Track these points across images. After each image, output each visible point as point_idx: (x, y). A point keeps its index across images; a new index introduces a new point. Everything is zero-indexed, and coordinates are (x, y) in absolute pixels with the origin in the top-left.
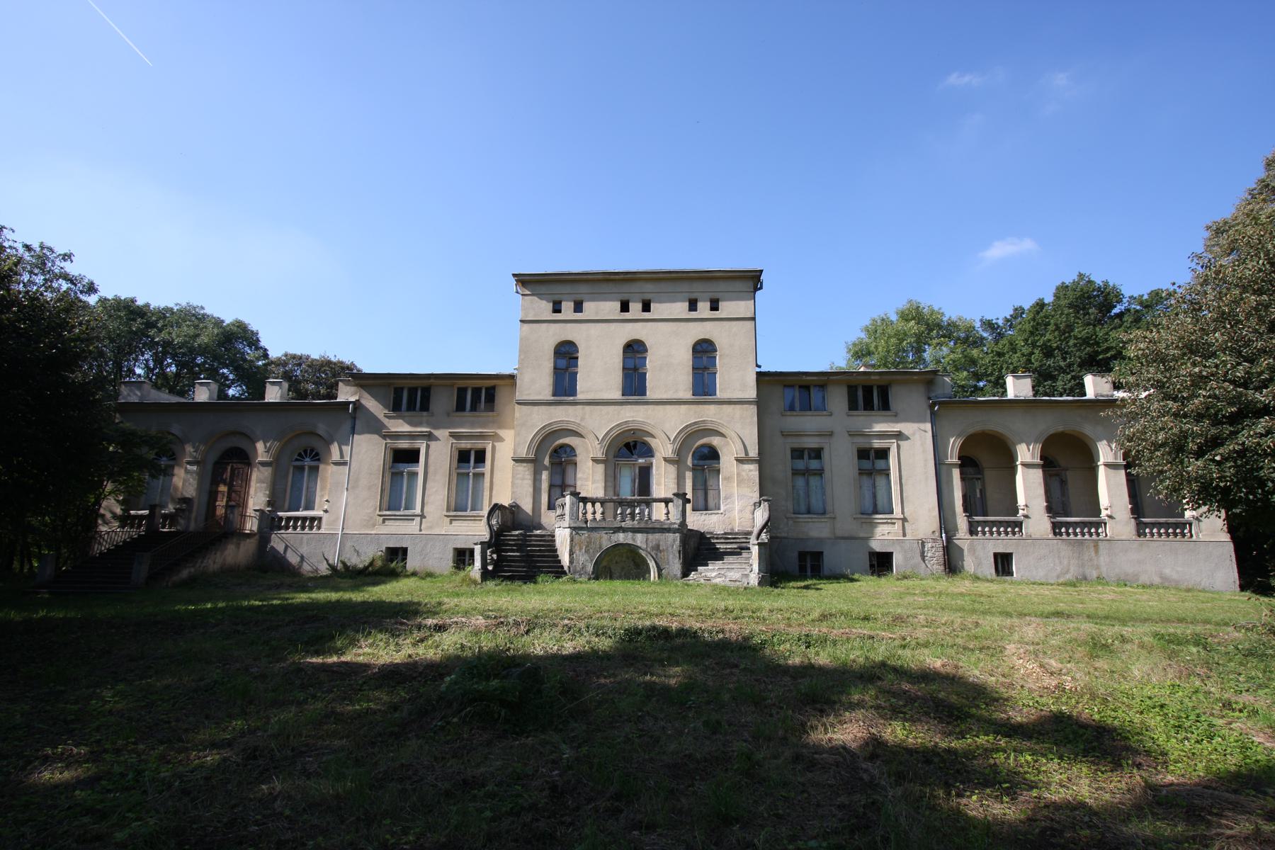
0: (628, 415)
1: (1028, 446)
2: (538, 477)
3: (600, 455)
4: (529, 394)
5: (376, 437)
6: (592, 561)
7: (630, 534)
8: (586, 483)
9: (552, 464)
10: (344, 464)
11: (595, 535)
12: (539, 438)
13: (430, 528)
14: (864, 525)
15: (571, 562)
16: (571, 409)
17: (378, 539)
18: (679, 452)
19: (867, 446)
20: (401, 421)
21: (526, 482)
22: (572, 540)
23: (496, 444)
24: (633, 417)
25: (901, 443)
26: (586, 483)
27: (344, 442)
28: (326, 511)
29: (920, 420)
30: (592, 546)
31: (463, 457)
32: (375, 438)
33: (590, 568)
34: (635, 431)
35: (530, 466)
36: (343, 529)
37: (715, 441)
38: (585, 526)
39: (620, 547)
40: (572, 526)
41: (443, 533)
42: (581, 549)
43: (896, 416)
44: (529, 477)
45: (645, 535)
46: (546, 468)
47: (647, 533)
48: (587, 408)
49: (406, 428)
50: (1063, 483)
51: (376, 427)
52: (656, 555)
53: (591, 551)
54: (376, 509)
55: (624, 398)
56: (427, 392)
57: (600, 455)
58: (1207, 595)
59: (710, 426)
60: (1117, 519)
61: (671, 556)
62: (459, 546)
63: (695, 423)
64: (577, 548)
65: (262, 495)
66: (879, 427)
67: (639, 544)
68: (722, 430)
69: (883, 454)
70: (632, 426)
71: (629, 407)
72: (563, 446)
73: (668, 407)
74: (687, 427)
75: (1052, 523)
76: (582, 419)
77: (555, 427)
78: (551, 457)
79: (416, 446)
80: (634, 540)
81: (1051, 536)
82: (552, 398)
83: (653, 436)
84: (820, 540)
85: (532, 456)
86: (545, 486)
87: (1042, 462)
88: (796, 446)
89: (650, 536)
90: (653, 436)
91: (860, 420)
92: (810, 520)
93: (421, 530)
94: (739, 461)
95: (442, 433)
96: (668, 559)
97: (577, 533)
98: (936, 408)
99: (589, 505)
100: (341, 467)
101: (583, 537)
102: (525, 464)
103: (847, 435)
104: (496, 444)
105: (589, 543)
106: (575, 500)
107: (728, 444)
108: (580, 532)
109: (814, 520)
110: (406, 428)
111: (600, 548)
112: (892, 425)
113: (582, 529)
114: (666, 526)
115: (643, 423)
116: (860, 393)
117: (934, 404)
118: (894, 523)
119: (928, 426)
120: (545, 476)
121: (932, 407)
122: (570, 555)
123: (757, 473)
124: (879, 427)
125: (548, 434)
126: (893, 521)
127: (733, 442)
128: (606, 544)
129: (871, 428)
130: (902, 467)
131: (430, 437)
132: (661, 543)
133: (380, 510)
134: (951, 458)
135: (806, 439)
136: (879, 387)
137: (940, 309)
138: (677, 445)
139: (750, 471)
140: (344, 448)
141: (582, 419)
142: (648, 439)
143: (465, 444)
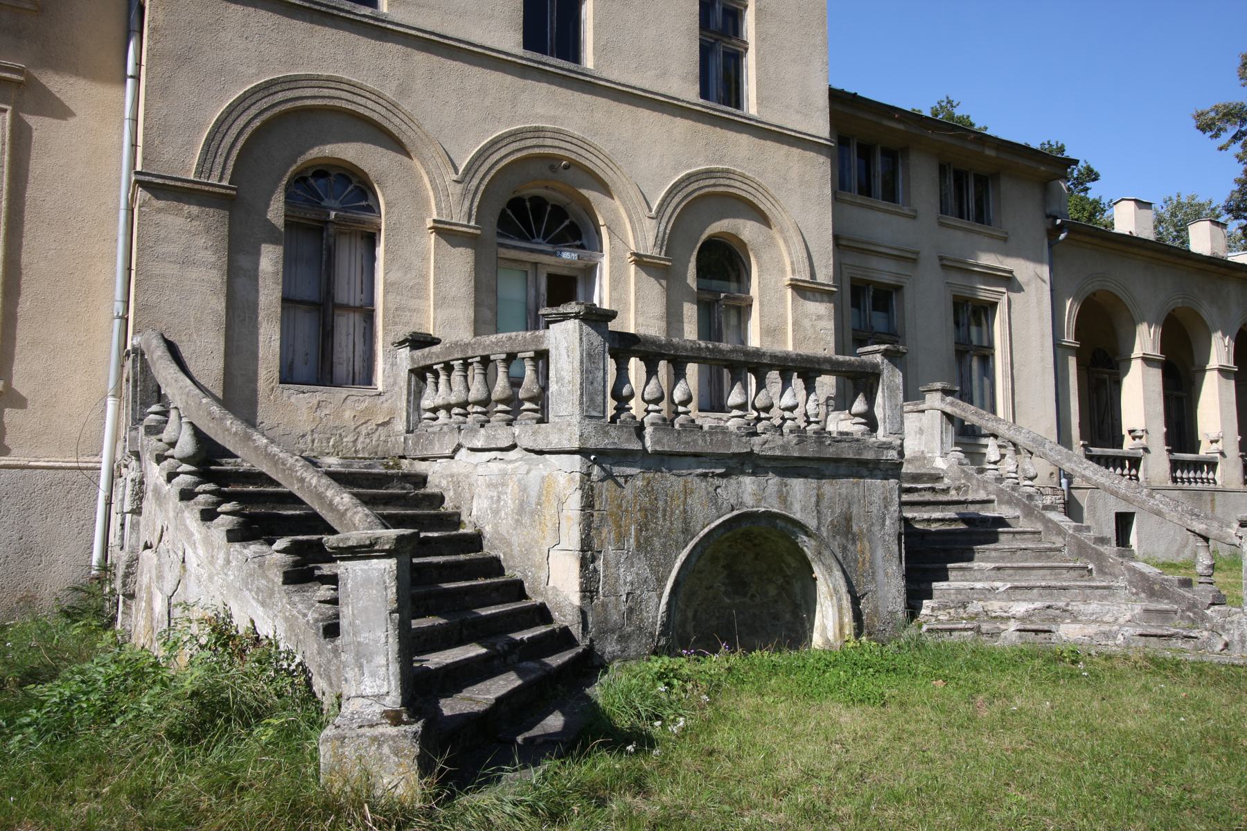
0: (540, 110)
1: (1150, 327)
2: (244, 261)
3: (459, 216)
6: (661, 581)
7: (773, 481)
8: (413, 303)
9: (291, 224)
11: (671, 482)
12: (248, 121)
15: (588, 591)
16: (365, 47)
18: (672, 241)
19: (967, 294)
21: (194, 273)
22: (588, 504)
23: (31, 120)
24: (554, 119)
25: (1013, 296)
26: (413, 303)
29: (1037, 260)
30: (661, 524)
33: (657, 608)
34: (551, 162)
35: (216, 218)
37: (747, 230)
38: (636, 446)
39: (745, 526)
40: (592, 444)
42: (621, 537)
43: (1005, 240)
44: (209, 257)
45: (813, 483)
46: (272, 236)
47: (820, 476)
48: (422, 59)
52: (844, 549)
53: (657, 543)
55: (529, 54)
57: (459, 216)
59: (739, 189)
60: (1228, 458)
61: (880, 553)
63: (709, 173)
64: (607, 534)
66: (988, 260)
67: (798, 516)
68: (765, 205)
69: (989, 308)
70: (550, 146)
71: (543, 88)
73: (645, 114)
74: (689, 179)
75: (1171, 461)
76: (403, 91)
77: (309, 96)
78: (289, 197)
80: (784, 499)
81: (1170, 484)
83: (605, 189)
85: (219, 179)
86: (269, 295)
87: (1162, 358)
88: (859, 274)
89: (828, 487)
90: (605, 189)
91: (956, 240)
94: (800, 289)
96: (872, 563)
97: (609, 476)
98: (1062, 236)
99: (635, 367)
101: (628, 491)
102: (195, 210)
103: (937, 263)
104: (31, 120)
105: (649, 513)
106: (597, 340)
107: (771, 243)
108: (616, 470)
111: (687, 532)
112: (1001, 258)
113: (624, 456)
114: (869, 455)
115: (583, 143)
117: (1060, 229)
119: (1045, 271)
120: (269, 260)
121: (1053, 232)
122: (584, 564)
123: (830, 325)
124: (988, 260)
125: (287, 113)
127: (786, 241)
128: (707, 521)
129: (976, 258)
130: (1014, 345)
132: (855, 510)
134: (1068, 337)
135: (875, 263)
138: (666, 225)
139: (819, 317)
141: (403, 91)
142: (592, 195)
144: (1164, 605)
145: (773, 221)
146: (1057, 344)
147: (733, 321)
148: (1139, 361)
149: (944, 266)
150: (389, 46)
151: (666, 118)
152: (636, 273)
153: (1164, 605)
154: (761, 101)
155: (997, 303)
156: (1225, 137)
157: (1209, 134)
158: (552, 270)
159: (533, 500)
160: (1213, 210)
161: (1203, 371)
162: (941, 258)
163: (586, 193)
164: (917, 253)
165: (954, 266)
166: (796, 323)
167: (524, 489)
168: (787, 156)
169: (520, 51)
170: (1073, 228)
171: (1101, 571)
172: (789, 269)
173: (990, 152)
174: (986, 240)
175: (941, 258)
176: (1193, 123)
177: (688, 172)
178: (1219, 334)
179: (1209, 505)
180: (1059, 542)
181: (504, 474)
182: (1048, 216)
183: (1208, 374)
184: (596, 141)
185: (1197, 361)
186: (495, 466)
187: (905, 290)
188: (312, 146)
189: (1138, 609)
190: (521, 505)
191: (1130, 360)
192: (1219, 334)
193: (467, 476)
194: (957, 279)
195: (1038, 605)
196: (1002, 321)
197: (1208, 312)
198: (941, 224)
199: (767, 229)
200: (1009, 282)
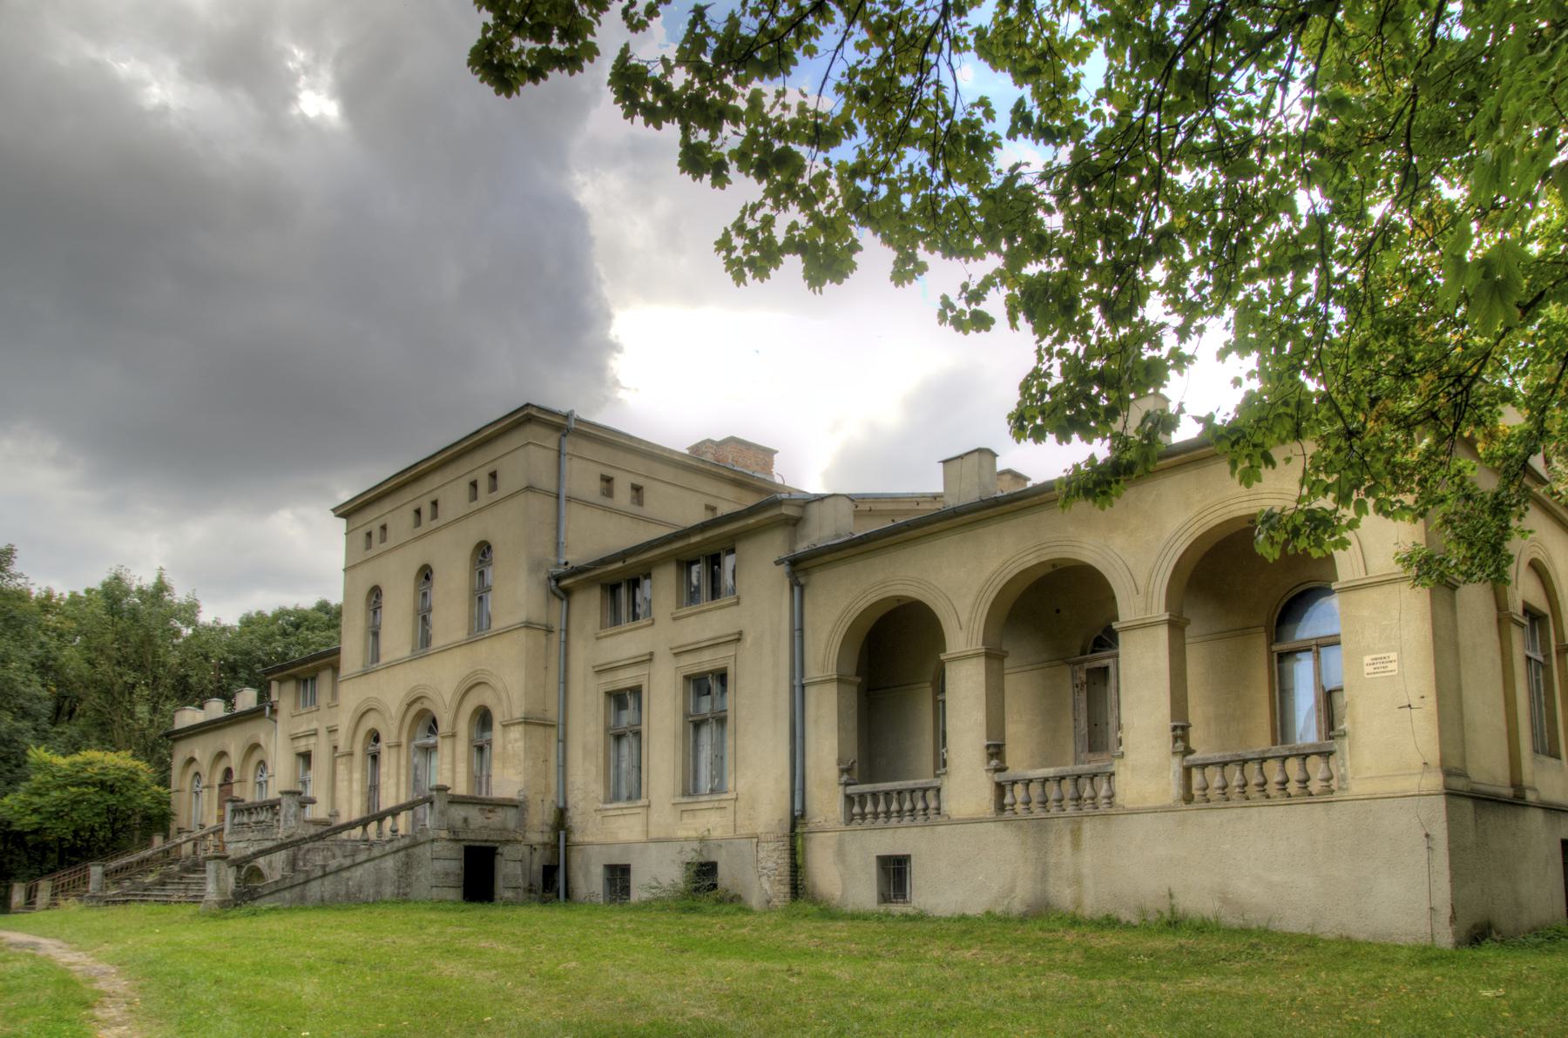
14: (685, 815)
50: (1001, 690)
84: (627, 846)
92: (619, 812)
109: (625, 811)
126: (723, 804)
179: (1067, 839)
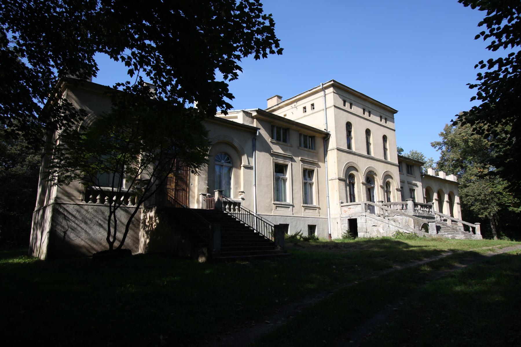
4: (340, 145)
5: (268, 154)
10: (251, 168)
13: (297, 213)
17: (275, 219)
20: (278, 146)
27: (250, 155)
28: (243, 199)
29: (420, 182)
31: (305, 171)
32: (267, 155)
36: (256, 213)
41: (303, 216)
43: (415, 178)
49: (280, 151)
51: (267, 149)
54: (271, 200)
56: (286, 131)
58: (78, 223)
62: (310, 224)
65: (203, 183)
66: (414, 182)
72: (351, 174)
73: (379, 163)
79: (286, 163)
82: (348, 150)
87: (438, 199)
93: (293, 214)
95: (298, 159)
98: (424, 177)
100: (249, 170)
102: (342, 182)
107: (393, 182)
110: (280, 151)
116: (311, 148)
117: (423, 175)
118: (289, 207)
121: (422, 176)
127: (395, 182)
131: (292, 160)
133: (274, 201)
136: (281, 141)
137: (440, 137)
140: (250, 159)
143: (307, 166)
144: (467, 235)
145: (393, 178)
146: (424, 197)
147: (309, 187)
148: (446, 202)
149: (408, 183)
150: (356, 156)
151: (381, 163)
152: (362, 187)
153: (467, 235)
154: (374, 153)
155: (314, 170)
156: (437, 148)
157: (434, 147)
158: (368, 187)
159: (407, 221)
160: (422, 155)
161: (443, 201)
162: (408, 182)
163: (374, 176)
164: (404, 181)
165: (410, 183)
166: (397, 195)
167: (406, 220)
168: (394, 167)
169: (367, 155)
170: (425, 175)
171: (457, 232)
172: (395, 186)
173: (414, 162)
174: (413, 178)
175: (408, 182)
176: (431, 145)
177: (385, 171)
178: (446, 194)
180: (449, 228)
181: (403, 218)
182: (421, 173)
183: (444, 202)
184: (375, 168)
185: (442, 199)
186: (401, 217)
187: (404, 188)
188: (351, 171)
189: (463, 236)
190: (406, 221)
191: (433, 199)
192: (446, 194)
193: (397, 218)
194: (410, 185)
195: (452, 235)
196: (416, 193)
197: (444, 190)
198: (407, 175)
199: (357, 172)
200: (416, 185)
